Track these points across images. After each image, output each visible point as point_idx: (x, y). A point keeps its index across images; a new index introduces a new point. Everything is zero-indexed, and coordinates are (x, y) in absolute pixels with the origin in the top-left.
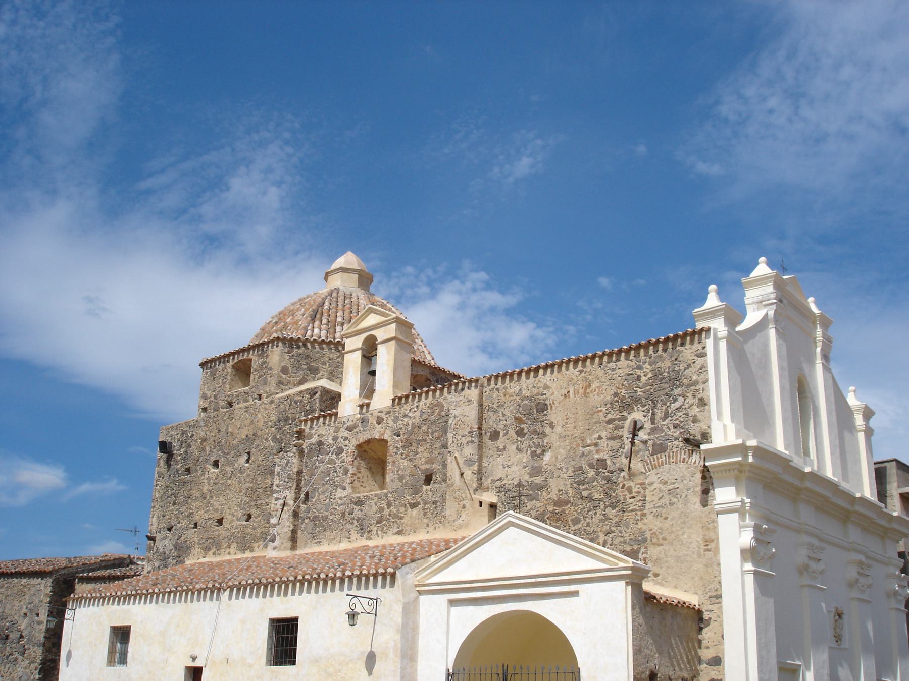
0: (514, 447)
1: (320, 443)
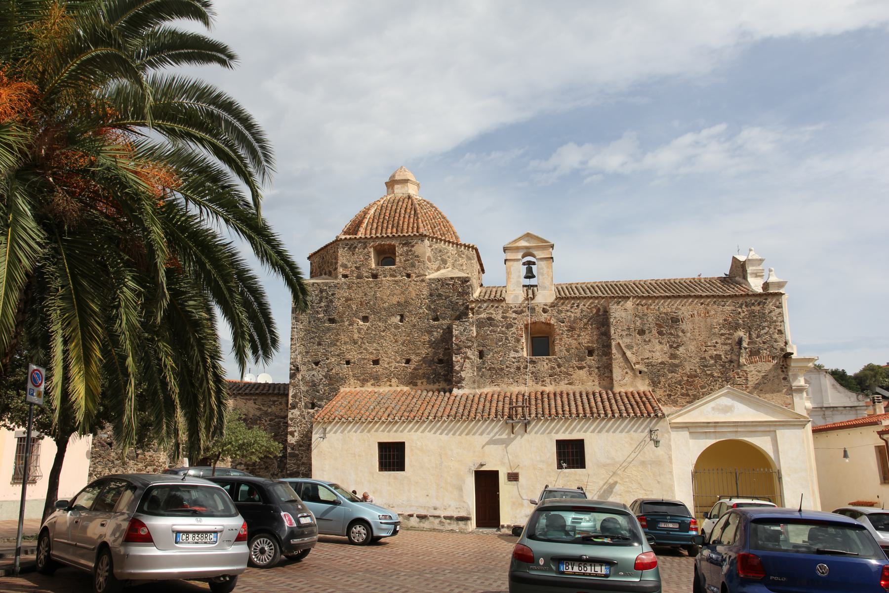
1: (490, 319)
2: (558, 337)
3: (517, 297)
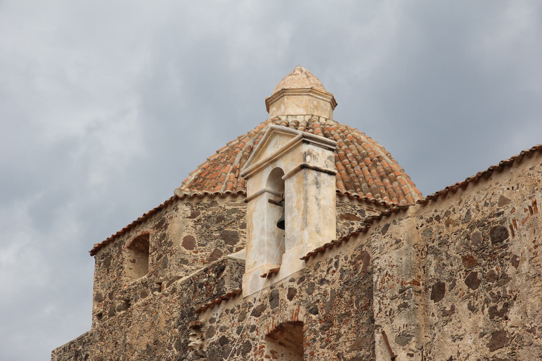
0: (465, 305)
1: (223, 341)
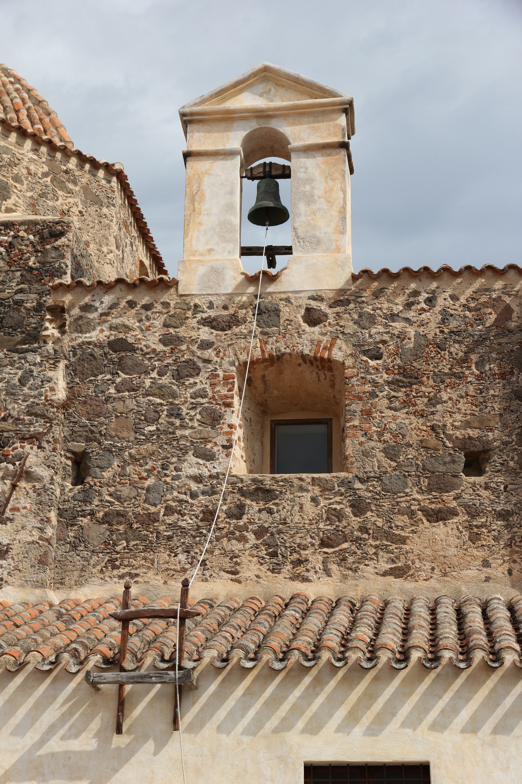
1: (119, 346)
2: (357, 407)
3: (217, 272)
